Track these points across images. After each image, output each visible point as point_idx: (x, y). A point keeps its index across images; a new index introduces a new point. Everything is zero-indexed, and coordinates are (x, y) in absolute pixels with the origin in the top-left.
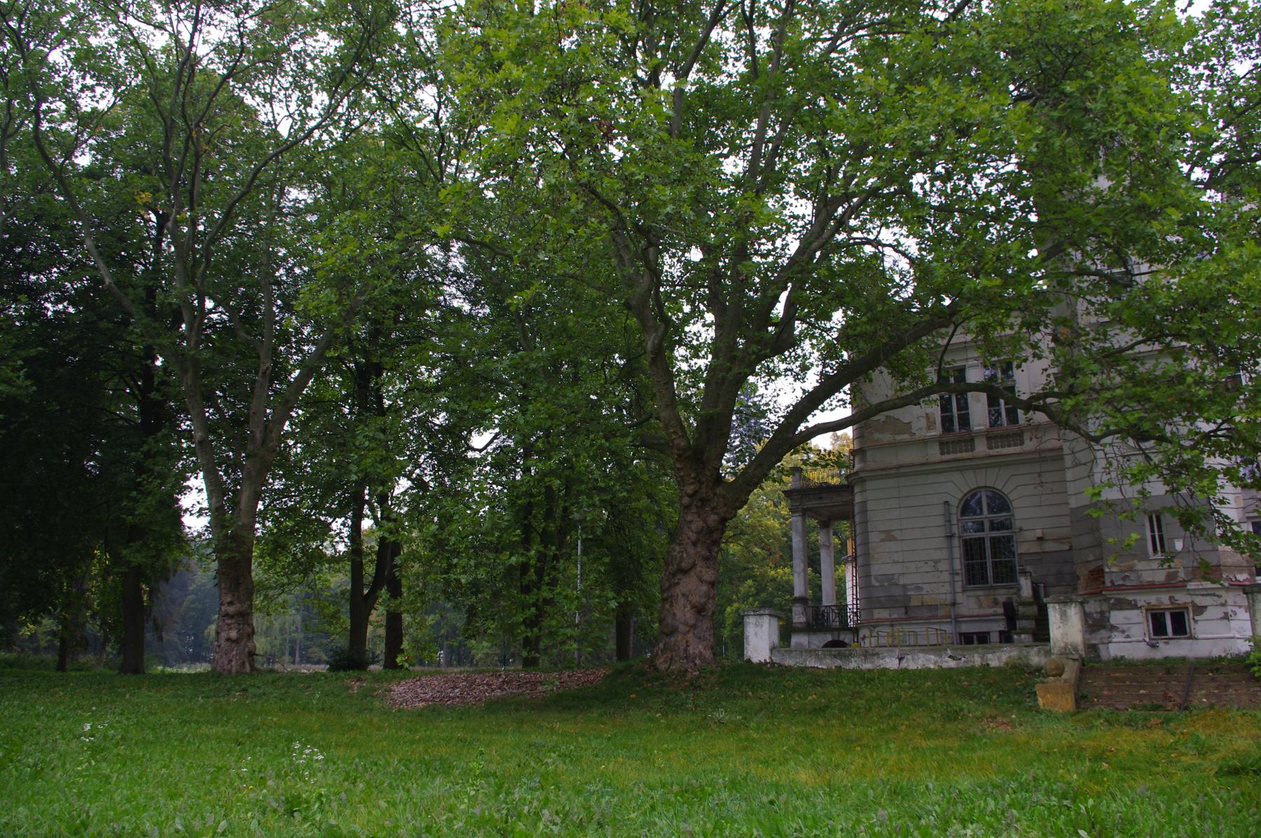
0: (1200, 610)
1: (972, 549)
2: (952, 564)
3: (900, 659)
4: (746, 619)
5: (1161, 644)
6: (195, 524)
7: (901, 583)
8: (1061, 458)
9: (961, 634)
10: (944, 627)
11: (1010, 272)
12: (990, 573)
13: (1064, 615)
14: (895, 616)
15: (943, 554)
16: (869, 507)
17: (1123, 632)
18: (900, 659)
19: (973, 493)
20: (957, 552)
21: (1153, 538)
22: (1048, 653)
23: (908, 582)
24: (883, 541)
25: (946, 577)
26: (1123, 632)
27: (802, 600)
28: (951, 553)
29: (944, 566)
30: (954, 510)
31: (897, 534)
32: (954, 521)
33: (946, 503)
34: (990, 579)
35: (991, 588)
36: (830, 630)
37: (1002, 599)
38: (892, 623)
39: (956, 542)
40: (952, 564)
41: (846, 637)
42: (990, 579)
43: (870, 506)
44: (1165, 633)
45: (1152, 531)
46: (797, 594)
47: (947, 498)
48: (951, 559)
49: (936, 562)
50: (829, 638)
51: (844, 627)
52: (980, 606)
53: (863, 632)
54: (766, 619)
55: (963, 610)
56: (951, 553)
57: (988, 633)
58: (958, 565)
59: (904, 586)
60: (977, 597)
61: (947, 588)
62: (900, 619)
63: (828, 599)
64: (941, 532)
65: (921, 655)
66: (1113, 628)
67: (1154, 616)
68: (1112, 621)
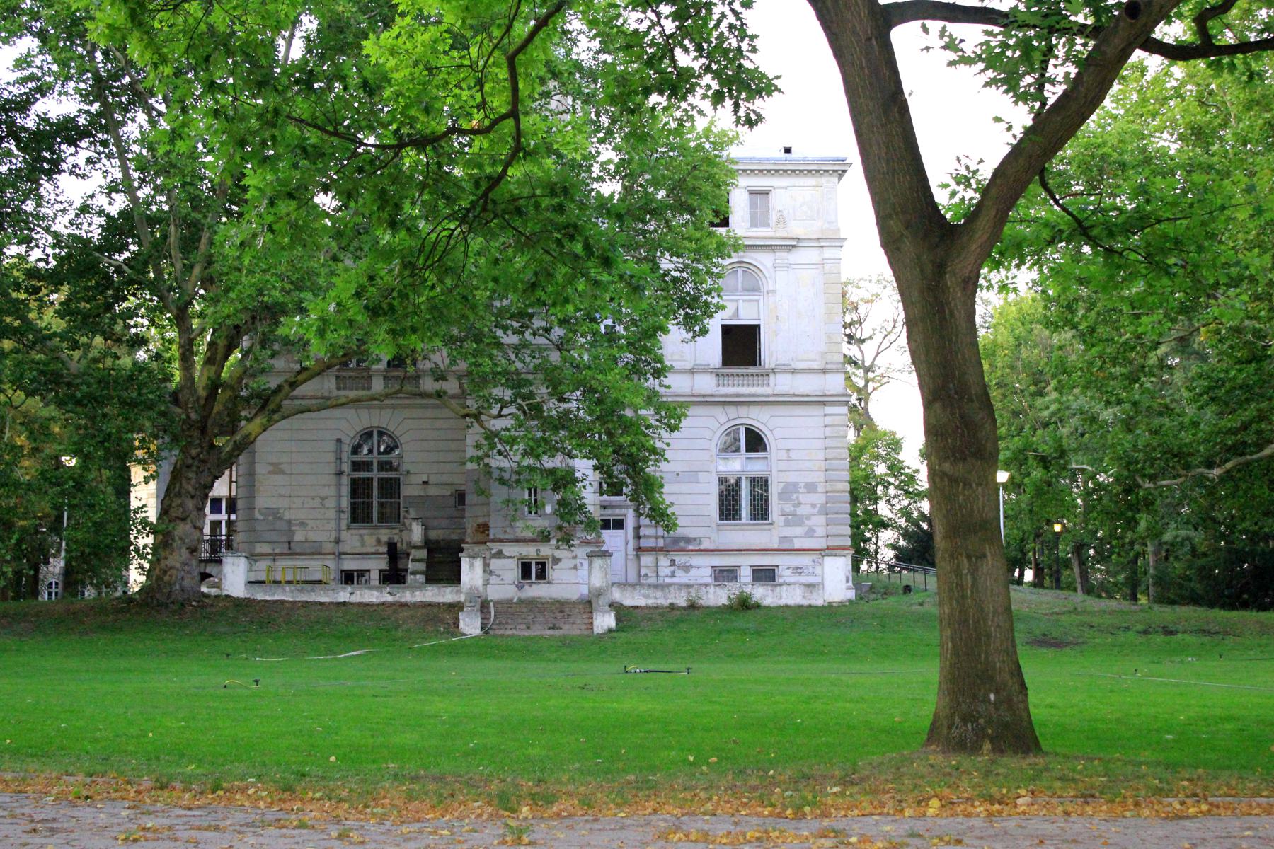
1: (359, 489)
5: (526, 587)
13: (472, 565)
14: (277, 551)
15: (331, 491)
20: (346, 491)
25: (332, 514)
29: (331, 503)
31: (285, 467)
33: (339, 440)
39: (345, 480)
44: (530, 578)
49: (323, 499)
59: (289, 522)
61: (333, 525)
62: (281, 554)
64: (332, 469)
67: (523, 564)
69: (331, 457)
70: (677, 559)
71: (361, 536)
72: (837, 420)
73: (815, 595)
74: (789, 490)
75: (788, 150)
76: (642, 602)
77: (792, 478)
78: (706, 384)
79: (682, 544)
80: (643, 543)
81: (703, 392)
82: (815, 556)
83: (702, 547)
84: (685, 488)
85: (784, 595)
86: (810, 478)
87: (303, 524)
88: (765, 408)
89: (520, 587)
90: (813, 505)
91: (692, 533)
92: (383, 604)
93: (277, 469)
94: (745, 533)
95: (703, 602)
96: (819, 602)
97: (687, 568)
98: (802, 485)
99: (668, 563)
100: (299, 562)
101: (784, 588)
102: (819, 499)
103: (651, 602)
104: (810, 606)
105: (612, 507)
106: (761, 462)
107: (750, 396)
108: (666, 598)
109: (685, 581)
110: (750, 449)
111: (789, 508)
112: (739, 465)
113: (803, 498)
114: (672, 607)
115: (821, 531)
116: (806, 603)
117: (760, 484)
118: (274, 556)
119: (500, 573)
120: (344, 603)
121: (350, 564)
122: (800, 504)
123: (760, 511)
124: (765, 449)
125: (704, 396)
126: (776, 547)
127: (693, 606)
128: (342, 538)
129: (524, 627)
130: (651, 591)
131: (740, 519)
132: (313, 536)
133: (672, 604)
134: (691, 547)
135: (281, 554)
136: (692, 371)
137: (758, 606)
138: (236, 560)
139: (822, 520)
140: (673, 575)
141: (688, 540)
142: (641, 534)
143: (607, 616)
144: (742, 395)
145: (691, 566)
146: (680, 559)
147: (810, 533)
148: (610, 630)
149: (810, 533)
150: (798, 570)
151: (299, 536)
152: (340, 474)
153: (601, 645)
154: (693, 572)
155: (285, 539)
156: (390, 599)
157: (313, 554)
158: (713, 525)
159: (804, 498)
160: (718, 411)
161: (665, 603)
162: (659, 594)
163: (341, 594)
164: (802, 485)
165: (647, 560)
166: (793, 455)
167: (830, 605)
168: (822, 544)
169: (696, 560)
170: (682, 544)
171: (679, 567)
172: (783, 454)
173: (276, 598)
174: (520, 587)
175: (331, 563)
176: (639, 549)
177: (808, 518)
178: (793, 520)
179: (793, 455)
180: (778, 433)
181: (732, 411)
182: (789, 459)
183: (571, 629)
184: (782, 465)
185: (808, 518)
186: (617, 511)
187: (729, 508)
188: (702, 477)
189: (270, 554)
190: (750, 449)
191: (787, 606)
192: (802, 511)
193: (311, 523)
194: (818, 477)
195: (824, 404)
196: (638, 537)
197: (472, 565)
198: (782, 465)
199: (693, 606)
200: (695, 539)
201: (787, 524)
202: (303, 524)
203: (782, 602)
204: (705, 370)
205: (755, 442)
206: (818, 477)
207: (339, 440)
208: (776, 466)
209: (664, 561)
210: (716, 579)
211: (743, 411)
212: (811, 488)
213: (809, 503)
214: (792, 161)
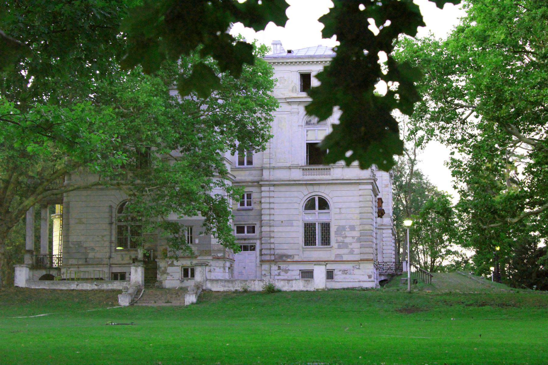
1: (120, 230)
2: (111, 238)
3: (77, 285)
4: (16, 268)
5: (185, 281)
7: (85, 245)
8: (121, 238)
9: (112, 273)
12: (129, 243)
13: (136, 271)
14: (80, 263)
15: (107, 233)
16: (71, 205)
17: (172, 276)
18: (77, 285)
20: (114, 232)
21: (188, 237)
22: (130, 284)
23: (88, 245)
24: (77, 223)
25: (107, 244)
26: (172, 276)
27: (30, 252)
28: (111, 232)
29: (107, 238)
30: (114, 210)
31: (84, 220)
32: (114, 216)
33: (111, 207)
34: (129, 246)
35: (128, 251)
36: (45, 268)
38: (78, 266)
39: (114, 226)
40: (111, 238)
41: (54, 273)
42: (129, 246)
43: (72, 204)
44: (188, 276)
45: (188, 234)
46: (27, 248)
49: (103, 236)
50: (44, 272)
51: (51, 267)
53: (63, 270)
54: (25, 268)
56: (111, 232)
57: (125, 273)
58: (113, 239)
59: (86, 248)
61: (107, 249)
62: (82, 265)
63: (44, 250)
64: (107, 221)
65: (85, 284)
66: (168, 274)
67: (184, 270)
68: (168, 271)
69: (107, 215)
70: (282, 266)
71: (122, 255)
72: (366, 192)
73: (309, 286)
74: (340, 229)
75: (289, 52)
76: (221, 289)
77: (342, 223)
78: (297, 175)
79: (284, 258)
80: (264, 258)
81: (295, 179)
82: (357, 263)
83: (295, 260)
84: (288, 229)
85: (294, 285)
86: (352, 223)
87: (93, 249)
88: (328, 187)
89: (182, 281)
90: (353, 237)
91: (289, 252)
92: (93, 290)
93: (80, 222)
94: (318, 252)
95: (249, 289)
96: (312, 289)
97: (286, 271)
98: (347, 227)
99: (277, 268)
100: (90, 269)
101: (294, 281)
102: (356, 234)
103: (226, 289)
104: (307, 291)
105: (249, 239)
106: (327, 215)
107: (319, 180)
108: (234, 287)
109: (286, 278)
110: (320, 208)
111: (340, 239)
112: (317, 217)
113: (347, 234)
114: (236, 292)
115: (357, 251)
116: (305, 289)
117: (326, 227)
118: (78, 266)
119: (173, 274)
120: (73, 290)
121: (116, 270)
122: (346, 237)
123: (326, 241)
124: (329, 208)
125: (295, 181)
126: (333, 259)
127: (245, 291)
128: (113, 256)
129: (153, 302)
130: (226, 284)
131: (315, 245)
132: (98, 255)
133: (236, 290)
134: (289, 260)
135: (82, 265)
136: (290, 168)
137: (279, 291)
138: (21, 268)
139: (358, 245)
140: (279, 275)
141: (288, 256)
142: (263, 253)
143: (191, 296)
144: (315, 180)
145: (289, 270)
146: (283, 266)
147: (352, 252)
148: (193, 304)
149: (352, 252)
150: (345, 272)
151: (91, 255)
152: (111, 224)
153: (123, 312)
154: (290, 273)
155: (84, 257)
156: (96, 287)
157: (98, 264)
158: (301, 248)
159: (349, 233)
160: (303, 188)
161: (233, 289)
162: (230, 285)
163: (72, 285)
164: (347, 227)
165: (266, 267)
166: (343, 211)
167: (317, 290)
168: (357, 258)
169: (291, 267)
170: (284, 258)
171: (283, 270)
172: (338, 211)
173: (41, 287)
174: (182, 281)
175: (106, 270)
176: (262, 261)
177: (351, 244)
178: (343, 245)
179: (343, 211)
180: (335, 199)
181: (311, 188)
182: (340, 213)
183: (176, 303)
184: (337, 217)
185: (351, 244)
186: (251, 241)
187: (309, 240)
188: (295, 223)
189: (76, 265)
190: (320, 208)
191: (295, 291)
192: (347, 240)
193: (97, 249)
194: (356, 223)
195: (359, 184)
196: (261, 255)
197: (136, 271)
198: (337, 217)
199: (245, 291)
200: (291, 256)
201: (339, 247)
202: (93, 249)
203: (293, 289)
204: (297, 167)
205: (324, 204)
206: (356, 223)
207: (111, 207)
208: (334, 217)
209: (274, 267)
210: (302, 277)
211: (316, 188)
212: (352, 228)
213: (351, 236)
214: (292, 58)
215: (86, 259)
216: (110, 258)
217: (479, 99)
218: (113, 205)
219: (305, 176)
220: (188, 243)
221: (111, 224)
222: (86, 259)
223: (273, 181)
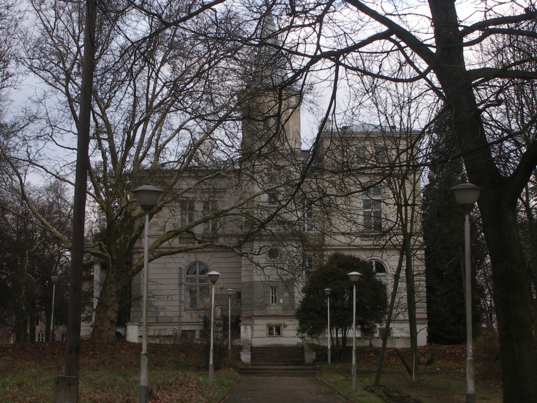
0: (285, 326)
4: (128, 326)
6: (490, 27)
10: (175, 327)
11: (535, 297)
13: (246, 329)
15: (177, 292)
19: (194, 264)
21: (272, 297)
25: (177, 303)
30: (183, 272)
33: (180, 268)
37: (202, 315)
45: (272, 294)
47: (180, 265)
48: (180, 295)
52: (192, 318)
55: (183, 320)
56: (180, 292)
60: (191, 313)
61: (177, 309)
62: (153, 323)
64: (177, 282)
69: (177, 276)
132: (169, 314)
197: (246, 329)
202: (164, 308)
215: (157, 317)
216: (180, 317)
217: (256, 175)
218: (183, 267)
219: (363, 242)
220: (273, 302)
221: (180, 284)
222: (157, 317)
223: (335, 246)
